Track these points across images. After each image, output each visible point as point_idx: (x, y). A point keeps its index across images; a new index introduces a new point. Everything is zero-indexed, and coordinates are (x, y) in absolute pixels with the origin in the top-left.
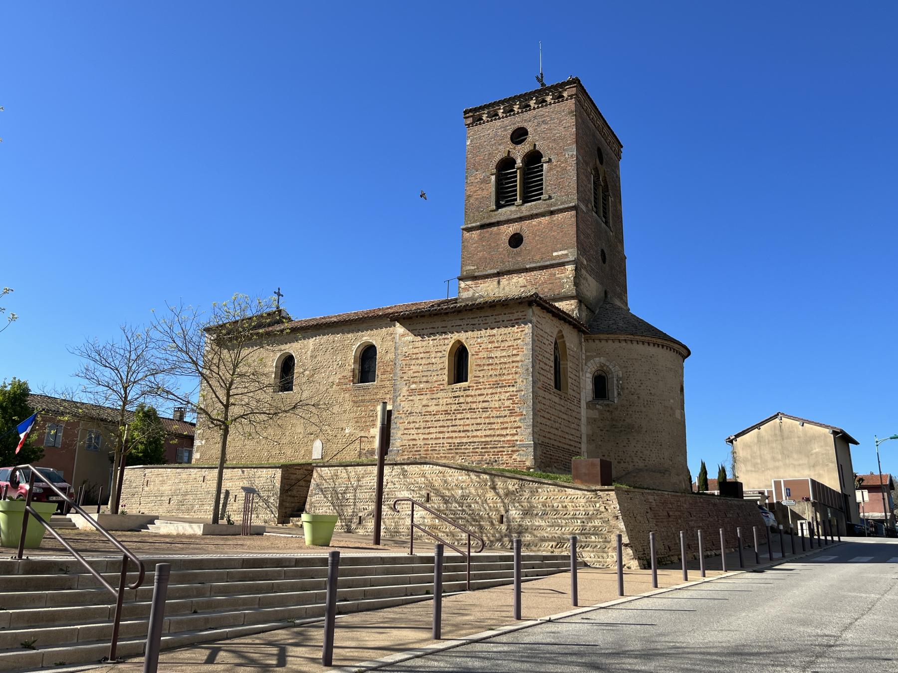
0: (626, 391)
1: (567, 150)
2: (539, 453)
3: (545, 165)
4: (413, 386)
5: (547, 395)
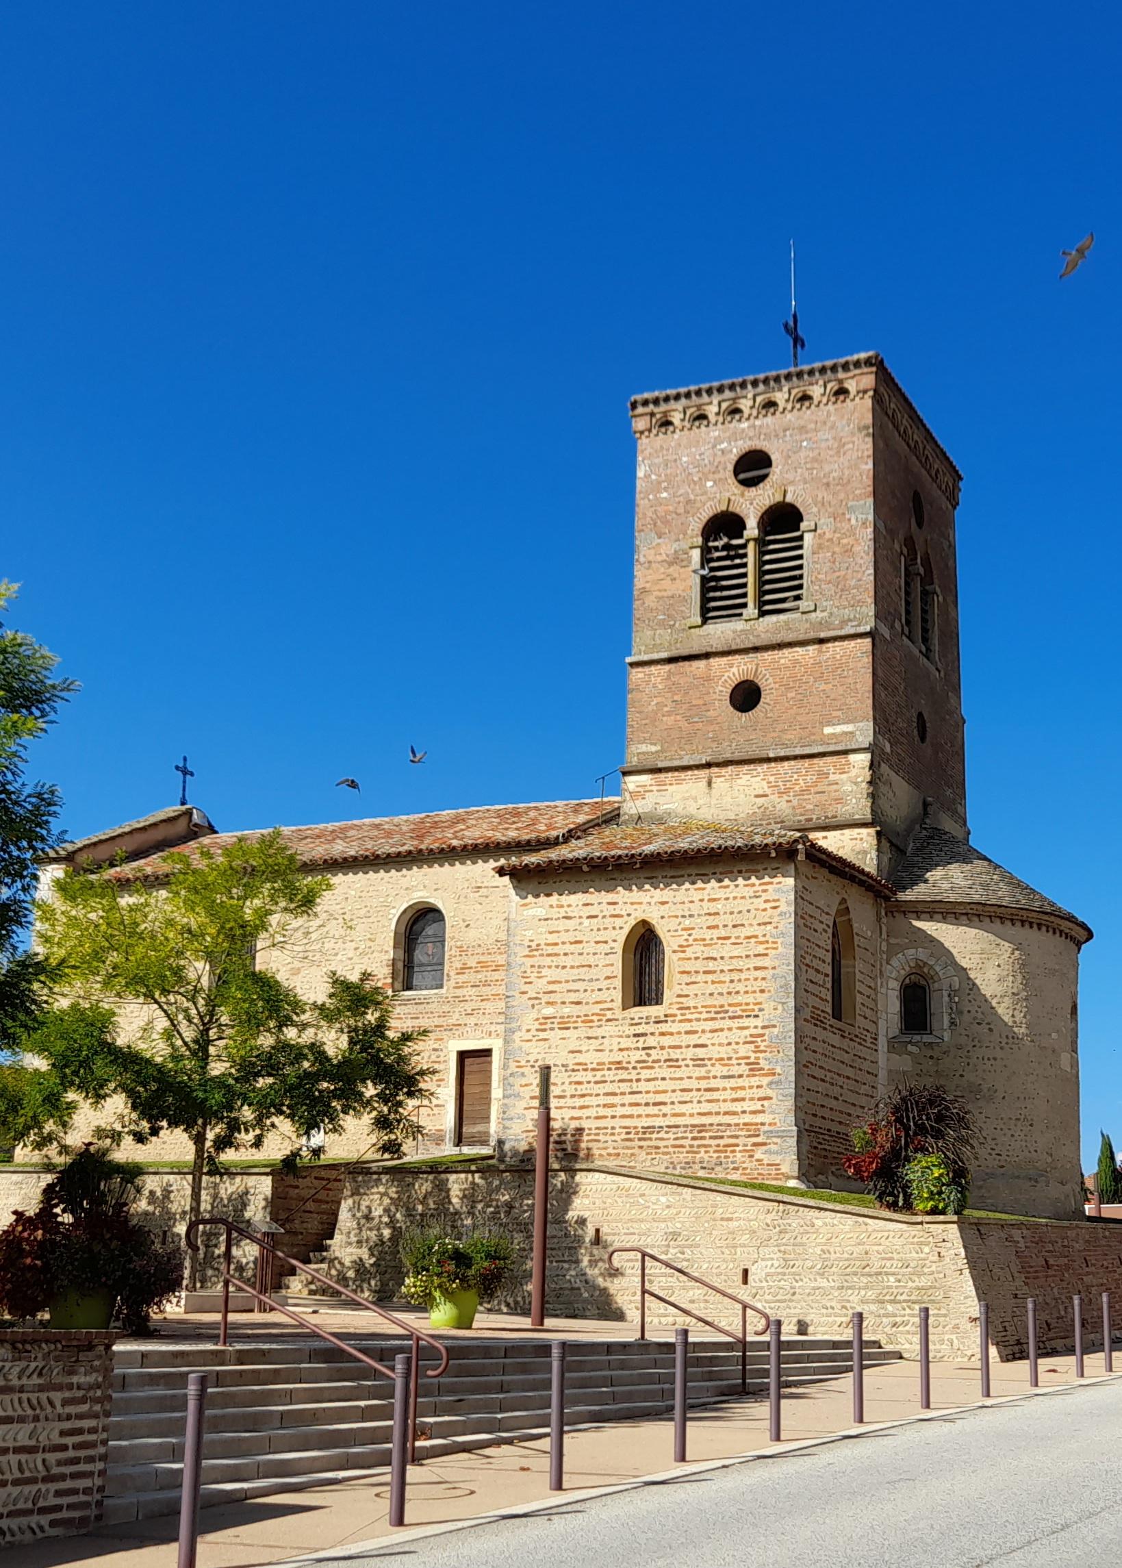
0: (966, 1018)
2: (805, 1149)
3: (807, 537)
4: (549, 1011)
5: (820, 1034)
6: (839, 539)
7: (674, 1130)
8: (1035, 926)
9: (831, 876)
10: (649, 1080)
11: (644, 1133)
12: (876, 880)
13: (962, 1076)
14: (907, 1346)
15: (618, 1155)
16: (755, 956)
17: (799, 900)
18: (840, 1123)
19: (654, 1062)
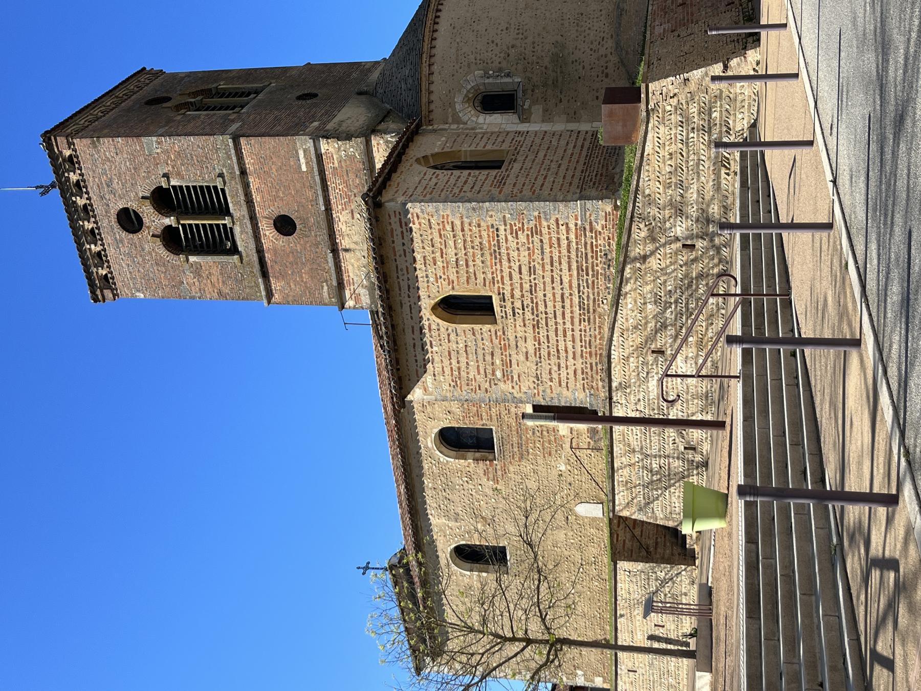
0: (504, 64)
2: (593, 193)
3: (173, 183)
4: (499, 374)
7: (582, 288)
8: (438, 14)
9: (399, 171)
10: (546, 306)
11: (584, 309)
12: (403, 136)
13: (546, 68)
14: (745, 122)
15: (600, 327)
17: (412, 198)
18: (578, 162)
19: (532, 302)
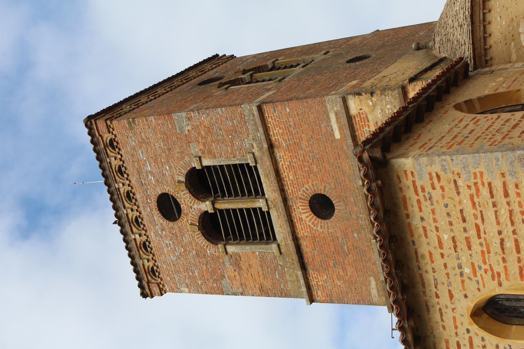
1: (181, 128)
6: (202, 138)
16: (492, 197)
